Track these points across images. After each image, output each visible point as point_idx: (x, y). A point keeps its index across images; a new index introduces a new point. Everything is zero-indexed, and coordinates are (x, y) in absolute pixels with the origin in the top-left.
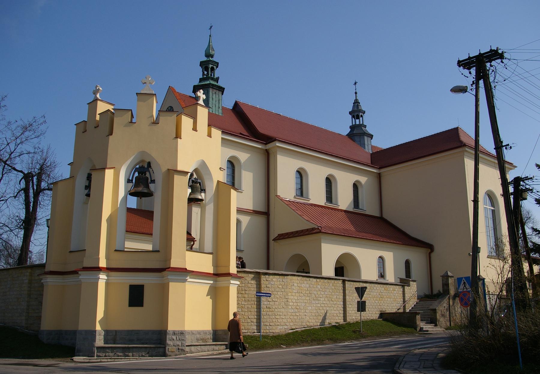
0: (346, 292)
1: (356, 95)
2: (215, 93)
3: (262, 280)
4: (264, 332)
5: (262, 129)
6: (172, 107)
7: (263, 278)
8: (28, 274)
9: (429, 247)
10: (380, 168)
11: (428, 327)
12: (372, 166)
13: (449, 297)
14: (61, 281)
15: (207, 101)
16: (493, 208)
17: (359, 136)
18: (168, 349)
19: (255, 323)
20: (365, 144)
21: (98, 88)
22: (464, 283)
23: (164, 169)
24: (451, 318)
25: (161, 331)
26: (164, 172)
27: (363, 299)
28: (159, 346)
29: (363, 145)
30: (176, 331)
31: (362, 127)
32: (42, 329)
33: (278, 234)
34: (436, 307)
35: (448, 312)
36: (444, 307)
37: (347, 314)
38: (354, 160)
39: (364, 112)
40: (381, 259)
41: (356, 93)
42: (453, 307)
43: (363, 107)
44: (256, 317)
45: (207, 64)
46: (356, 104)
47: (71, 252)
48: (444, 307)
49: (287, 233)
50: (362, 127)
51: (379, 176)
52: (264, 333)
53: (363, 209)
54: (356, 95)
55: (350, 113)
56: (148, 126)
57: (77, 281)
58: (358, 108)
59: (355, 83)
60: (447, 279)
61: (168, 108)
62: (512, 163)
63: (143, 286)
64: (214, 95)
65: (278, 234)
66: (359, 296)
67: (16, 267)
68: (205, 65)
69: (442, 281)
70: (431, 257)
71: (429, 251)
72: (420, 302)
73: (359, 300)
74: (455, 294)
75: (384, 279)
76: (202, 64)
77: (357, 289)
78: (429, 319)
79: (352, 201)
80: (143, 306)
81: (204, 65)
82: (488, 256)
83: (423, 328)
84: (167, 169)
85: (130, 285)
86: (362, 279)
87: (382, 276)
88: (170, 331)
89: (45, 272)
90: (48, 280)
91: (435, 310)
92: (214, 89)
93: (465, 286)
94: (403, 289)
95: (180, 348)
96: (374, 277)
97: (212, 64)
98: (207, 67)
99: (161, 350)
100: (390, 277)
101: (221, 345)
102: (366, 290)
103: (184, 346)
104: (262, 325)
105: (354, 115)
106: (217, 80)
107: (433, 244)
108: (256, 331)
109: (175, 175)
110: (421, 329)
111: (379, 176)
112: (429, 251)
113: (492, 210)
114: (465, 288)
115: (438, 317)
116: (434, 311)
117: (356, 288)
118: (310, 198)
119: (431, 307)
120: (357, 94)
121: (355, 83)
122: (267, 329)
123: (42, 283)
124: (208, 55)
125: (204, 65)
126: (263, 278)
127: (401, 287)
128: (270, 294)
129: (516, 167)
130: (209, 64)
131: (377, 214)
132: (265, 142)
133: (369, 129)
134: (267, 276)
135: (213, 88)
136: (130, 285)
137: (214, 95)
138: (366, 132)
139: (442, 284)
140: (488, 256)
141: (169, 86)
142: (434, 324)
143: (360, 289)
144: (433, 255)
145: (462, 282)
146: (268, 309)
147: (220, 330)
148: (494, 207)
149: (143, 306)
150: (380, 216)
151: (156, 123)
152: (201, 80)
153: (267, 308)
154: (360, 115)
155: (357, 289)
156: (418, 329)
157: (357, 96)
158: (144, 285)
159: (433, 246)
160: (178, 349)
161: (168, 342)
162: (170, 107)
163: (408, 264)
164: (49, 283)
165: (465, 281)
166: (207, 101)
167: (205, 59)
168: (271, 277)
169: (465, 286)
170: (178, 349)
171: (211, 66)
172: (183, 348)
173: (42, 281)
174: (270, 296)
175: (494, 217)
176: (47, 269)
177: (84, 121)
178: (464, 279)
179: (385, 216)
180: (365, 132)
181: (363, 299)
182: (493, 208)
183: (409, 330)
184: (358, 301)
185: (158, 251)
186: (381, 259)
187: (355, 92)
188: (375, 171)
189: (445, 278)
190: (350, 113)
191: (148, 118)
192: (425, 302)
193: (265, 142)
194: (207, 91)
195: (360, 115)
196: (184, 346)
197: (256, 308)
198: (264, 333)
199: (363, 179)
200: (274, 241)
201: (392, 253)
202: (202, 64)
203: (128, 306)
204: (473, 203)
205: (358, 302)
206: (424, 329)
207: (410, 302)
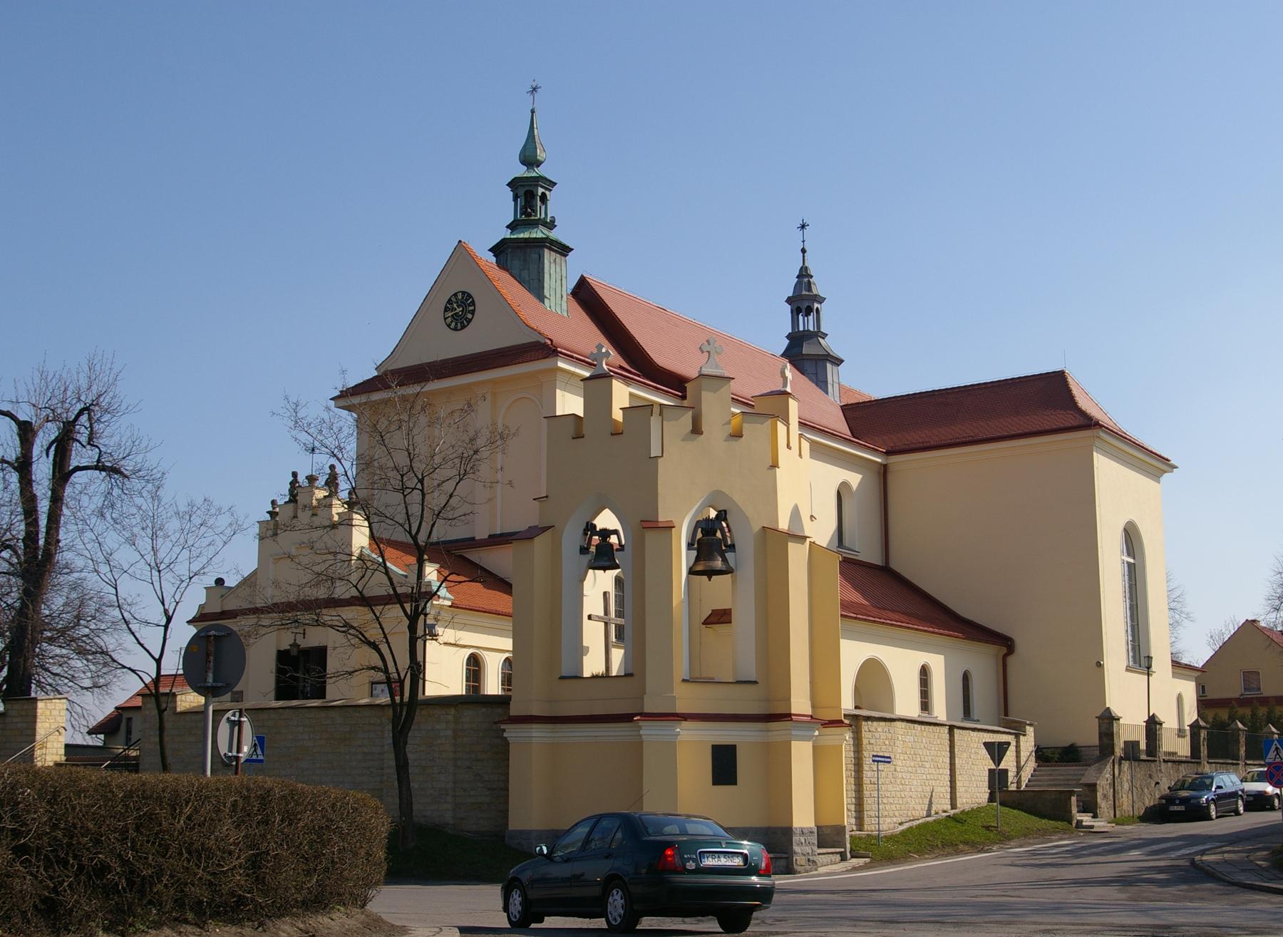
0: (956, 750)
1: (804, 257)
2: (555, 260)
3: (863, 730)
4: (869, 829)
5: (663, 357)
6: (470, 296)
7: (865, 726)
8: (450, 718)
9: (1006, 644)
10: (888, 453)
11: (1086, 819)
12: (873, 448)
13: (1114, 760)
14: (542, 734)
15: (539, 281)
16: (1131, 561)
17: (814, 362)
18: (796, 860)
19: (853, 813)
20: (827, 382)
21: (604, 350)
22: (1277, 748)
23: (756, 528)
24: (1117, 801)
25: (769, 828)
26: (756, 533)
27: (1002, 766)
28: (778, 855)
29: (822, 383)
30: (804, 828)
31: (819, 339)
32: (511, 827)
33: (712, 610)
34: (1096, 780)
35: (1112, 790)
36: (1107, 780)
37: (958, 794)
38: (843, 436)
39: (821, 300)
40: (925, 672)
41: (803, 251)
42: (1119, 780)
43: (819, 288)
44: (853, 800)
45: (531, 185)
46: (806, 280)
47: (562, 678)
48: (1107, 780)
49: (725, 610)
50: (819, 339)
51: (884, 471)
52: (868, 831)
53: (854, 549)
54: (804, 257)
55: (789, 301)
56: (725, 441)
57: (596, 736)
58: (810, 289)
59: (803, 227)
60: (1109, 723)
61: (455, 295)
62: (1169, 459)
63: (734, 747)
64: (553, 265)
65: (712, 610)
66: (993, 759)
67: (1189, 759)
68: (527, 188)
69: (1099, 726)
70: (1006, 665)
71: (1004, 650)
72: (1039, 768)
73: (993, 767)
74: (157, 680)
75: (928, 714)
76: (514, 184)
77: (988, 746)
78: (1081, 804)
79: (835, 531)
80: (735, 783)
81: (524, 186)
82: (1128, 668)
83: (1082, 821)
84: (761, 527)
85: (713, 746)
86: (897, 714)
87: (925, 705)
88: (796, 828)
89: (510, 716)
90: (534, 735)
91: (1095, 785)
92: (552, 252)
93: (1278, 753)
94: (1016, 742)
95: (811, 858)
96: (914, 711)
97: (542, 187)
98: (532, 192)
99: (783, 862)
100: (940, 710)
101: (832, 853)
102: (1008, 748)
103: (815, 855)
104: (865, 816)
105: (800, 306)
106: (551, 225)
107: (1013, 637)
108: (854, 828)
109: (789, 543)
110: (1079, 823)
111: (884, 471)
112: (1004, 650)
113: (1128, 563)
114: (1278, 756)
115: (1099, 800)
116: (1092, 787)
117: (986, 744)
118: (857, 550)
119: (1084, 780)
120: (806, 254)
121: (803, 227)
122: (872, 824)
123: (506, 738)
124: (529, 159)
125: (524, 186)
126: (865, 726)
127: (1013, 736)
128: (889, 758)
129: (1176, 467)
130: (537, 186)
131: (876, 560)
132: (680, 394)
133: (832, 344)
134: (870, 723)
135: (550, 249)
136: (713, 746)
137: (553, 265)
138: (831, 354)
139: (1100, 733)
140: (1128, 668)
141: (460, 241)
142: (1091, 814)
143: (996, 746)
144: (1011, 660)
145: (1273, 748)
146: (872, 786)
147: (826, 826)
148: (1134, 558)
149: (735, 783)
150: (884, 565)
151: (737, 435)
152: (512, 227)
153: (871, 784)
154: (815, 308)
155: (988, 746)
156: (1074, 822)
157: (806, 258)
158: (735, 746)
159: (1013, 641)
160: (809, 860)
161: (796, 848)
162: (463, 293)
163: (966, 678)
164: (533, 739)
165: (256, 742)
166: (539, 281)
167: (521, 171)
168: (875, 724)
169: (1278, 753)
170: (809, 860)
171: (540, 190)
172: (815, 858)
173: (505, 735)
174: (889, 762)
175: (1133, 579)
176: (515, 710)
177: (574, 414)
178: (1277, 743)
179: (895, 565)
180: (829, 354)
181: (1002, 766)
182: (1131, 561)
183: (1060, 824)
184: (989, 770)
185: (756, 682)
186: (925, 672)
187: (802, 247)
188: (879, 460)
189: (1106, 721)
190: (789, 301)
191: (724, 425)
192: (1053, 768)
193: (680, 394)
194: (538, 256)
195: (815, 308)
196: (815, 855)
197: (855, 785)
198: (868, 831)
199: (854, 479)
200: (704, 626)
201: (943, 656)
202: (514, 184)
203: (711, 783)
204: (714, 577)
205: (991, 771)
206: (1084, 824)
207: (1027, 769)
